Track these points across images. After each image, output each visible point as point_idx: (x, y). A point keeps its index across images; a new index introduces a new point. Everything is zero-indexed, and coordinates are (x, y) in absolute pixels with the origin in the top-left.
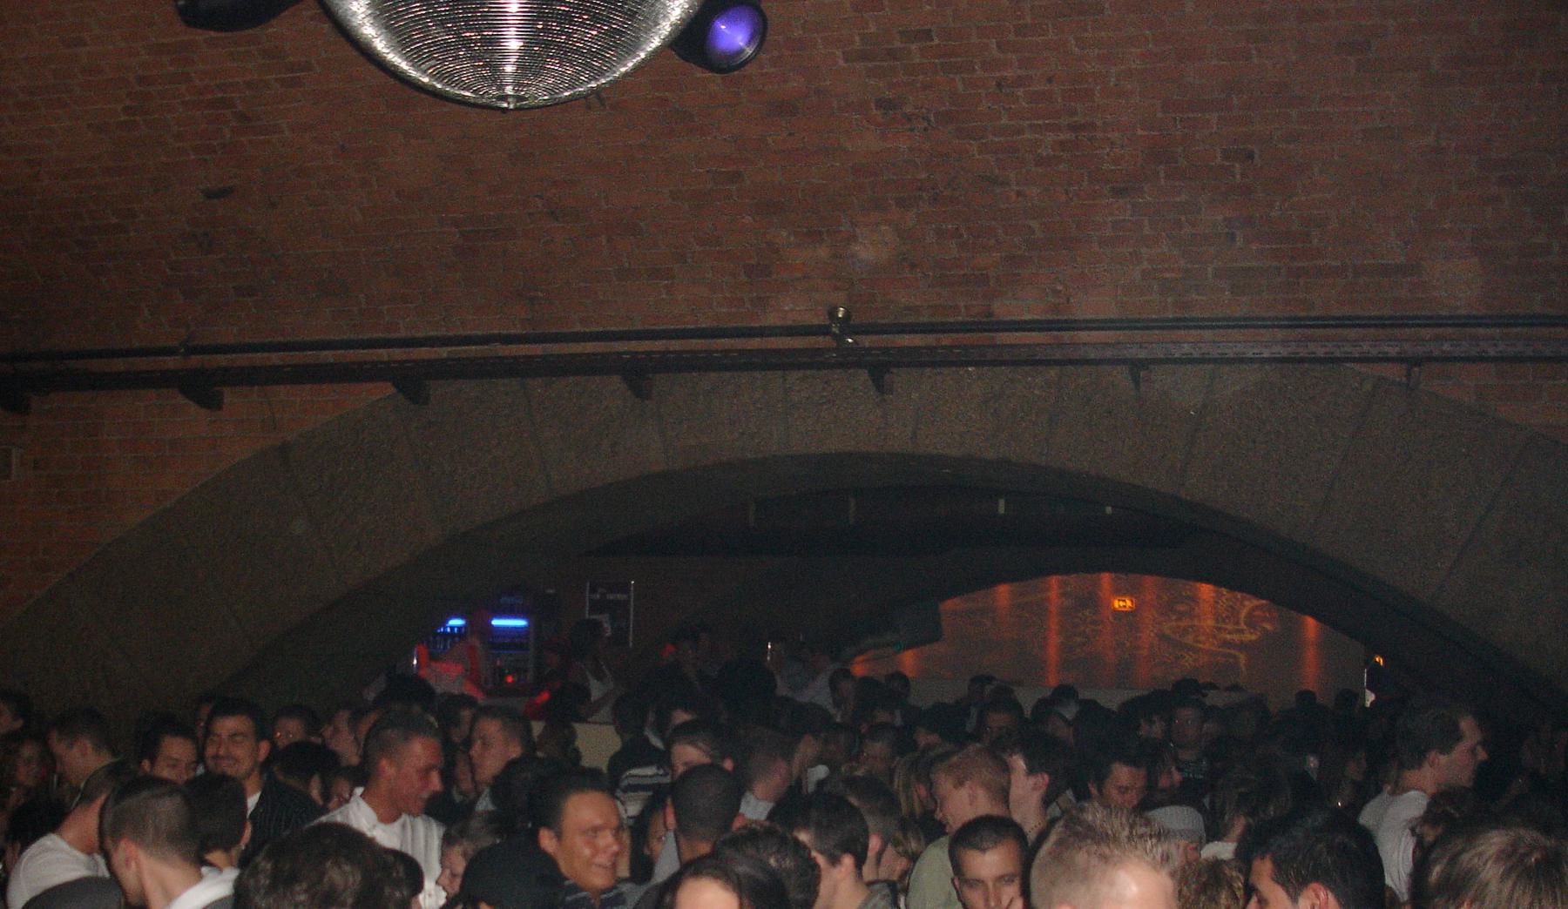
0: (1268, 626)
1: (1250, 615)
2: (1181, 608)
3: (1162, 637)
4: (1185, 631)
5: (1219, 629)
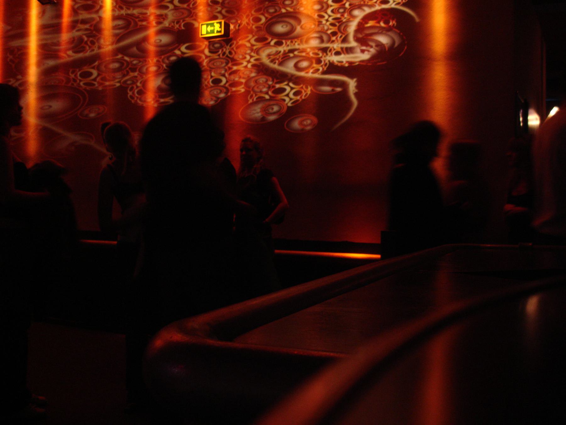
0: (384, 40)
1: (360, 28)
2: (280, 28)
3: (261, 68)
4: (285, 57)
5: (325, 50)
